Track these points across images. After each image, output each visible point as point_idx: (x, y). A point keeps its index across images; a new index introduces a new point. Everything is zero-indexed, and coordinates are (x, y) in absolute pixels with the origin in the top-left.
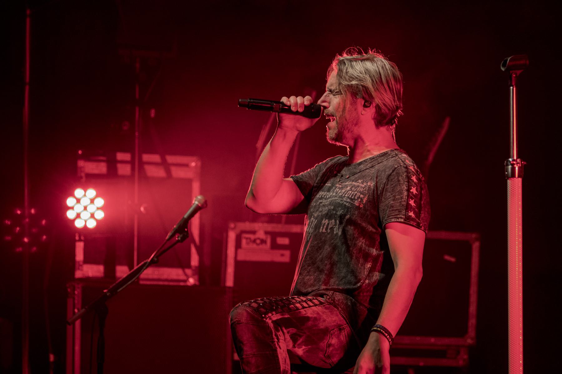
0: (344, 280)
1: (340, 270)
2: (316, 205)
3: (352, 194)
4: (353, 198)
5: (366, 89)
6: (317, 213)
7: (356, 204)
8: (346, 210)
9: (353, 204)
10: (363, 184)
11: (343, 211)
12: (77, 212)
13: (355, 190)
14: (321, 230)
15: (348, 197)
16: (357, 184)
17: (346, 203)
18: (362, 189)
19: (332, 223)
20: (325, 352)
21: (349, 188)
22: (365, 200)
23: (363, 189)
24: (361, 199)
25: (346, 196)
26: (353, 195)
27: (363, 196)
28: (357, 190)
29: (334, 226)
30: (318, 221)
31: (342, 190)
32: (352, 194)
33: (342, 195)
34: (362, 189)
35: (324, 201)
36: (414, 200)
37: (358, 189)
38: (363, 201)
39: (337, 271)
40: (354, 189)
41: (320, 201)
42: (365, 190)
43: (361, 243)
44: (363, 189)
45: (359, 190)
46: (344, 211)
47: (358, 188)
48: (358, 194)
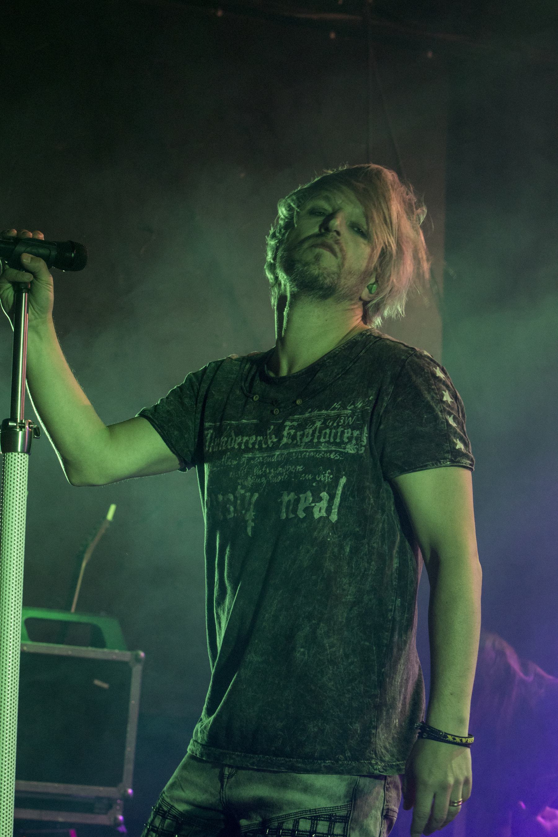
0: (356, 608)
1: (344, 590)
2: (238, 464)
3: (332, 435)
4: (338, 440)
5: (393, 190)
6: (249, 479)
7: (351, 452)
8: (335, 469)
9: (345, 453)
10: (347, 409)
11: (329, 471)
12: (351, 222)
13: (335, 424)
14: (284, 516)
15: (328, 442)
16: (333, 412)
17: (328, 454)
18: (350, 418)
19: (306, 498)
20: (355, 784)
21: (318, 424)
22: (365, 438)
23: (352, 418)
24: (357, 439)
25: (322, 440)
26: (336, 435)
27: (358, 432)
28: (340, 424)
29: (313, 505)
30: (260, 495)
31: (303, 430)
32: (332, 435)
33: (312, 440)
34: (350, 418)
35: (257, 456)
36: (452, 416)
37: (342, 421)
38: (361, 441)
39: (338, 592)
40: (333, 424)
41: (246, 456)
42: (358, 419)
43: (381, 525)
44: (352, 418)
45: (344, 422)
46: (332, 470)
47: (341, 419)
48: (346, 431)
